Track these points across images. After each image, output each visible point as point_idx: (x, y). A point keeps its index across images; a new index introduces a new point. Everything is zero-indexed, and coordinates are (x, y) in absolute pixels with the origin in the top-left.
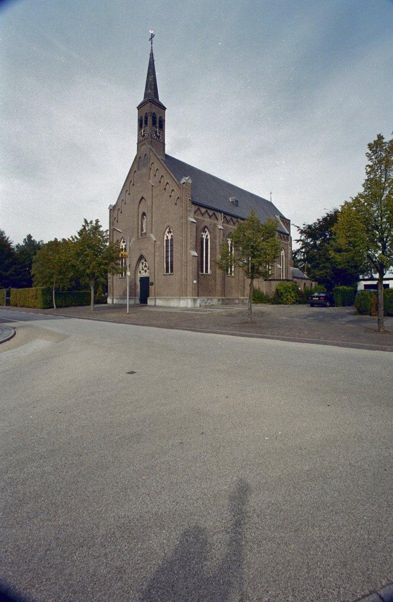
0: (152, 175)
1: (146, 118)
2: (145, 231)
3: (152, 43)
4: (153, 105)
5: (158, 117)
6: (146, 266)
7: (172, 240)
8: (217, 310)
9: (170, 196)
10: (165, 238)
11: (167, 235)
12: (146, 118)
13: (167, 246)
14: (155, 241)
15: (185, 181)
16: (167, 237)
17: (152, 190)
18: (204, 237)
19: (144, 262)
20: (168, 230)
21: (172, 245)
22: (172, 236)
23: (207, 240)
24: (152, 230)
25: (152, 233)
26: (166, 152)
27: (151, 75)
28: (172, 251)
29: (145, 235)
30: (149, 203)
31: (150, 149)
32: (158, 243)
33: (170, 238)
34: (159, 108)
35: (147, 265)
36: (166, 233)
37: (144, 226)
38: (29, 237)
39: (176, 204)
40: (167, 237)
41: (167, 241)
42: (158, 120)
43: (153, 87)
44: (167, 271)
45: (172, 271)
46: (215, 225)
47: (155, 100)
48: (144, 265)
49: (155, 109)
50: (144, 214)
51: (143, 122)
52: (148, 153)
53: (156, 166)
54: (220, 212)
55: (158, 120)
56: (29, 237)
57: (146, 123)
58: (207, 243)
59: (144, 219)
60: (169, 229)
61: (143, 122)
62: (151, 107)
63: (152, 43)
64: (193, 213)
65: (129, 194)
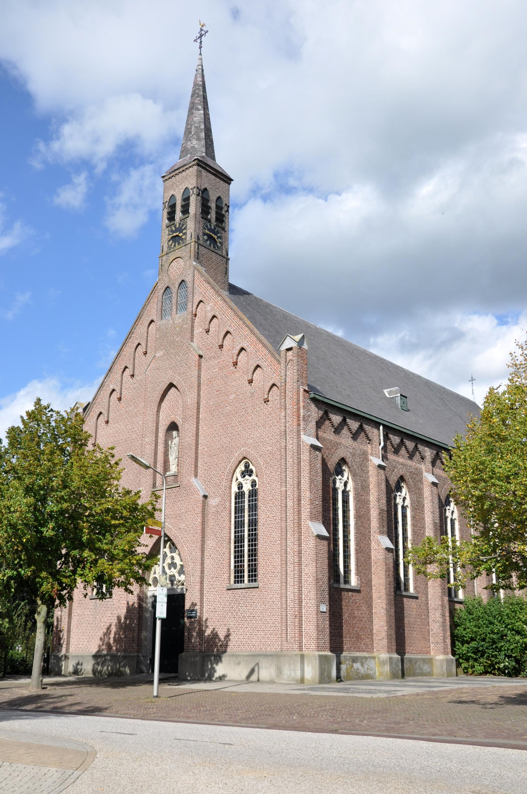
0: (198, 330)
1: (186, 200)
2: (173, 469)
3: (200, 47)
4: (204, 173)
5: (213, 197)
6: (173, 565)
7: (253, 493)
8: (406, 688)
9: (251, 382)
10: (235, 489)
11: (240, 479)
12: (186, 200)
13: (239, 510)
14: (205, 497)
15: (294, 345)
16: (240, 486)
17: (200, 365)
18: (340, 485)
19: (169, 555)
20: (242, 467)
21: (253, 508)
22: (254, 484)
23: (345, 493)
24: (196, 466)
25: (196, 476)
26: (229, 282)
27: (199, 110)
28: (253, 523)
29: (176, 481)
30: (191, 399)
31: (195, 268)
32: (213, 502)
33: (247, 487)
34: (218, 180)
35: (177, 560)
36: (238, 474)
37: (172, 458)
38: (233, 180)
39: (266, 401)
40: (240, 486)
41: (240, 495)
42: (213, 205)
43: (203, 135)
44: (239, 578)
45: (253, 577)
46: (364, 457)
47: (209, 162)
48: (168, 561)
49: (209, 181)
50: (173, 427)
51: (178, 209)
52: (189, 279)
53: (206, 310)
54: (376, 424)
55: (213, 205)
56: (233, 180)
57: (185, 210)
58: (346, 502)
59: (172, 438)
60: (247, 466)
61: (178, 209)
62: (199, 176)
63: (200, 47)
64: (314, 423)
65: (133, 376)
